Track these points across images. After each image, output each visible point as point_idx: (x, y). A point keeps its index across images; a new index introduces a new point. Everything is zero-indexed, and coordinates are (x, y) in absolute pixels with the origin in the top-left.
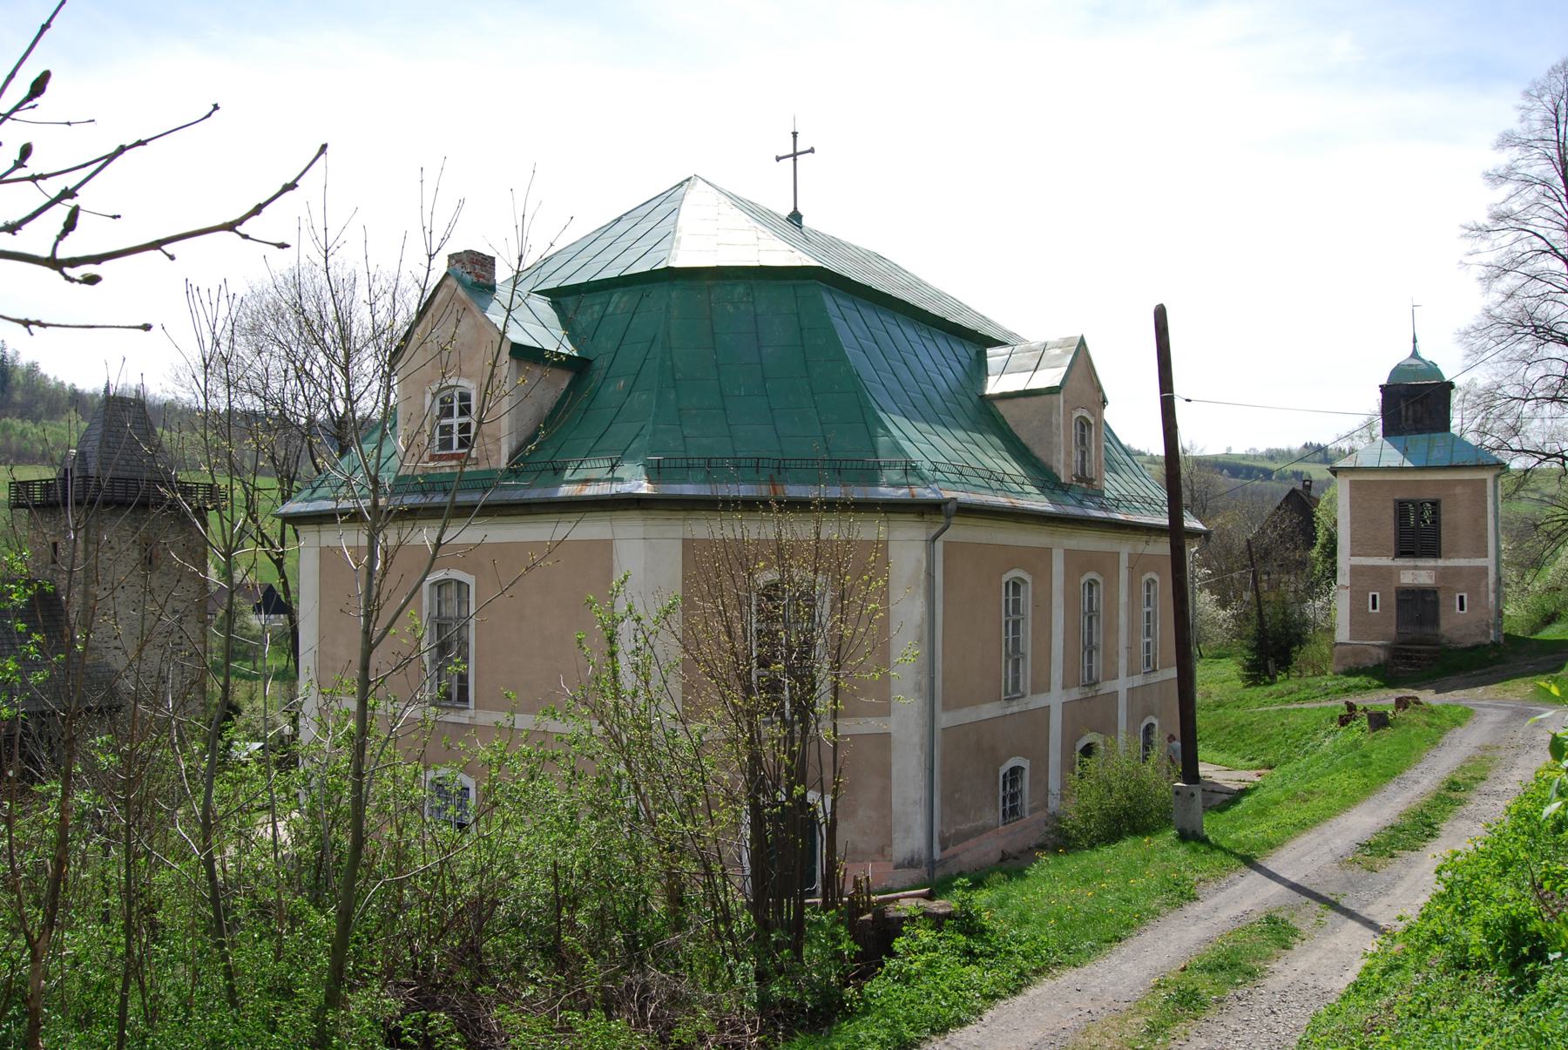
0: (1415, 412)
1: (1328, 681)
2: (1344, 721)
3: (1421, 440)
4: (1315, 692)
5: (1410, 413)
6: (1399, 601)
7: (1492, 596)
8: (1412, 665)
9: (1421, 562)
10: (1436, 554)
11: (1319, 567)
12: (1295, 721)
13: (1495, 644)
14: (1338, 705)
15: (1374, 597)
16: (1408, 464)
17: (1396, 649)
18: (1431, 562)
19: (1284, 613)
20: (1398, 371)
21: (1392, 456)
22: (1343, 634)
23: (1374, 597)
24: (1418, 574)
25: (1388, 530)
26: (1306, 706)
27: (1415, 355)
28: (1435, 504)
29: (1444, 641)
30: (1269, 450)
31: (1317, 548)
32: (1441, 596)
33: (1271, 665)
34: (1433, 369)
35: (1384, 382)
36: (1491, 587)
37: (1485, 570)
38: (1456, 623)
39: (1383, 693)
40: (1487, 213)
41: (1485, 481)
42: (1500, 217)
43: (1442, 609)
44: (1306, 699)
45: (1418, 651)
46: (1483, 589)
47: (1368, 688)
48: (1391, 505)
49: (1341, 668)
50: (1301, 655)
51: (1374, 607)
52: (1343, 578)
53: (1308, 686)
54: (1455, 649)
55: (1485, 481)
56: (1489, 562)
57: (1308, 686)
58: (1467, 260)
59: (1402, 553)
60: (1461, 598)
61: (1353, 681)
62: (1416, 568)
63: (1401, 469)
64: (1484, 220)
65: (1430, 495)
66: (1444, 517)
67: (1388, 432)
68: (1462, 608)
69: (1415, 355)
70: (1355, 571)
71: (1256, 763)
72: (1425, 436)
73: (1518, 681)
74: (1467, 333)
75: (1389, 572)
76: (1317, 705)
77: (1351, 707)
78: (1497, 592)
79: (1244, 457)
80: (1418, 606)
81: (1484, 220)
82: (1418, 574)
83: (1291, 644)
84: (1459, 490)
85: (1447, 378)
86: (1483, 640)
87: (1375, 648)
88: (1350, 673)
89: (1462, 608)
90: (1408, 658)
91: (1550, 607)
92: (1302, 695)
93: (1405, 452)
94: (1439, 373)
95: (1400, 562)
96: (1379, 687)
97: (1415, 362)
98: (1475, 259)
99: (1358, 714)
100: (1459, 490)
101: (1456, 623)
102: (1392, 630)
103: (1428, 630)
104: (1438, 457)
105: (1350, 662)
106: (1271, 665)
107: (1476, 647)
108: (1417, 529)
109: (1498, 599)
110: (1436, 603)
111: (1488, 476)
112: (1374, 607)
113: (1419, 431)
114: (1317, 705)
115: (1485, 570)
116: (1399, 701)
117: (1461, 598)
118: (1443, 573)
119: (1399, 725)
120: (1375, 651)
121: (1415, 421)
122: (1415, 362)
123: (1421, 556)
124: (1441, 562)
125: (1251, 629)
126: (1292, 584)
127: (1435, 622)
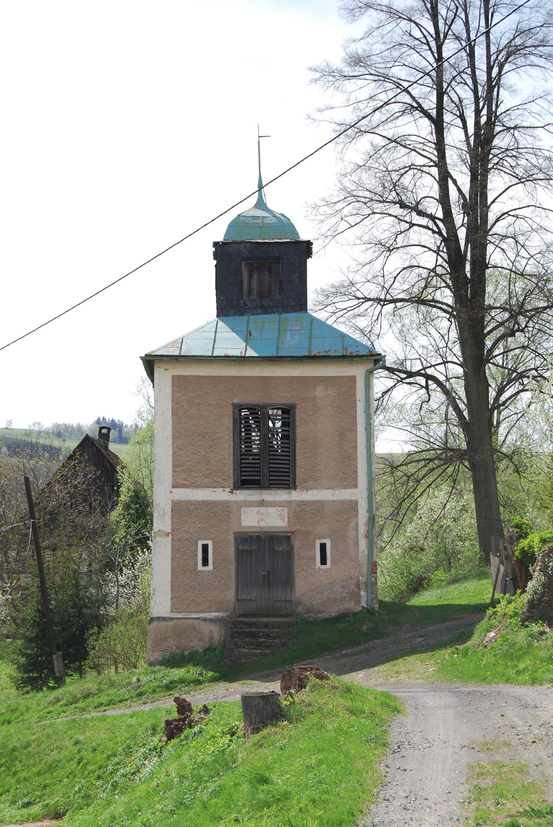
0: (260, 281)
1: (142, 674)
2: (173, 730)
3: (270, 321)
4: (124, 693)
5: (255, 284)
6: (240, 554)
7: (363, 543)
8: (259, 645)
9: (270, 495)
10: (287, 481)
11: (122, 533)
12: (96, 735)
13: (369, 612)
14: (166, 708)
15: (205, 548)
16: (251, 353)
17: (236, 624)
18: (282, 495)
19: (77, 586)
20: (237, 224)
21: (231, 343)
22: (161, 605)
23: (205, 548)
24: (264, 512)
25: (225, 454)
26: (111, 712)
27: (261, 204)
28: (288, 412)
29: (300, 609)
30: (57, 426)
31: (119, 509)
32: (297, 544)
33: (57, 662)
34: (286, 225)
35: (220, 238)
36: (362, 530)
37: (353, 506)
38: (316, 583)
39: (222, 687)
40: (342, 54)
41: (353, 379)
42: (357, 60)
43: (297, 563)
44: (111, 703)
45: (266, 625)
46: (351, 533)
47: (199, 682)
48: (229, 411)
49: (157, 656)
50: (97, 644)
51: (205, 562)
52: (162, 521)
53: (112, 684)
54: (315, 622)
55: (353, 379)
56: (359, 494)
57: (112, 684)
58: (318, 116)
59: (244, 482)
60: (323, 547)
61: (177, 673)
62: (262, 503)
63: (242, 360)
64: (337, 61)
65: (283, 397)
66: (301, 431)
67: (217, 317)
68: (323, 561)
69: (261, 204)
70: (179, 510)
71: (36, 809)
72: (274, 317)
73: (411, 659)
74: (316, 207)
75: (224, 511)
76: (129, 712)
77: (183, 707)
78: (369, 536)
79: (28, 433)
80: (265, 558)
81: (337, 61)
82: (264, 512)
83: (84, 628)
84: (320, 391)
85: (304, 236)
86: (351, 606)
87: (207, 623)
88: (172, 662)
89: (323, 561)
90: (252, 635)
91: (416, 568)
92: (104, 699)
93: (247, 337)
94: (290, 227)
95: (242, 495)
96: (214, 680)
97: (260, 213)
98: (327, 115)
99: (196, 716)
100: (320, 391)
101: (316, 583)
102: (231, 595)
103: (279, 594)
104: (293, 344)
105: (172, 645)
106: (57, 662)
107: (342, 617)
108: (264, 449)
109: (371, 545)
110: (289, 554)
111: (357, 371)
112: (205, 562)
113: (266, 310)
114: (129, 712)
115: (353, 506)
116: (248, 702)
117: (323, 547)
118: (299, 511)
119: (300, 717)
120: (206, 628)
121: (261, 295)
122: (260, 213)
123: (269, 487)
124: (296, 496)
125: (29, 611)
126: (82, 558)
127: (288, 581)
